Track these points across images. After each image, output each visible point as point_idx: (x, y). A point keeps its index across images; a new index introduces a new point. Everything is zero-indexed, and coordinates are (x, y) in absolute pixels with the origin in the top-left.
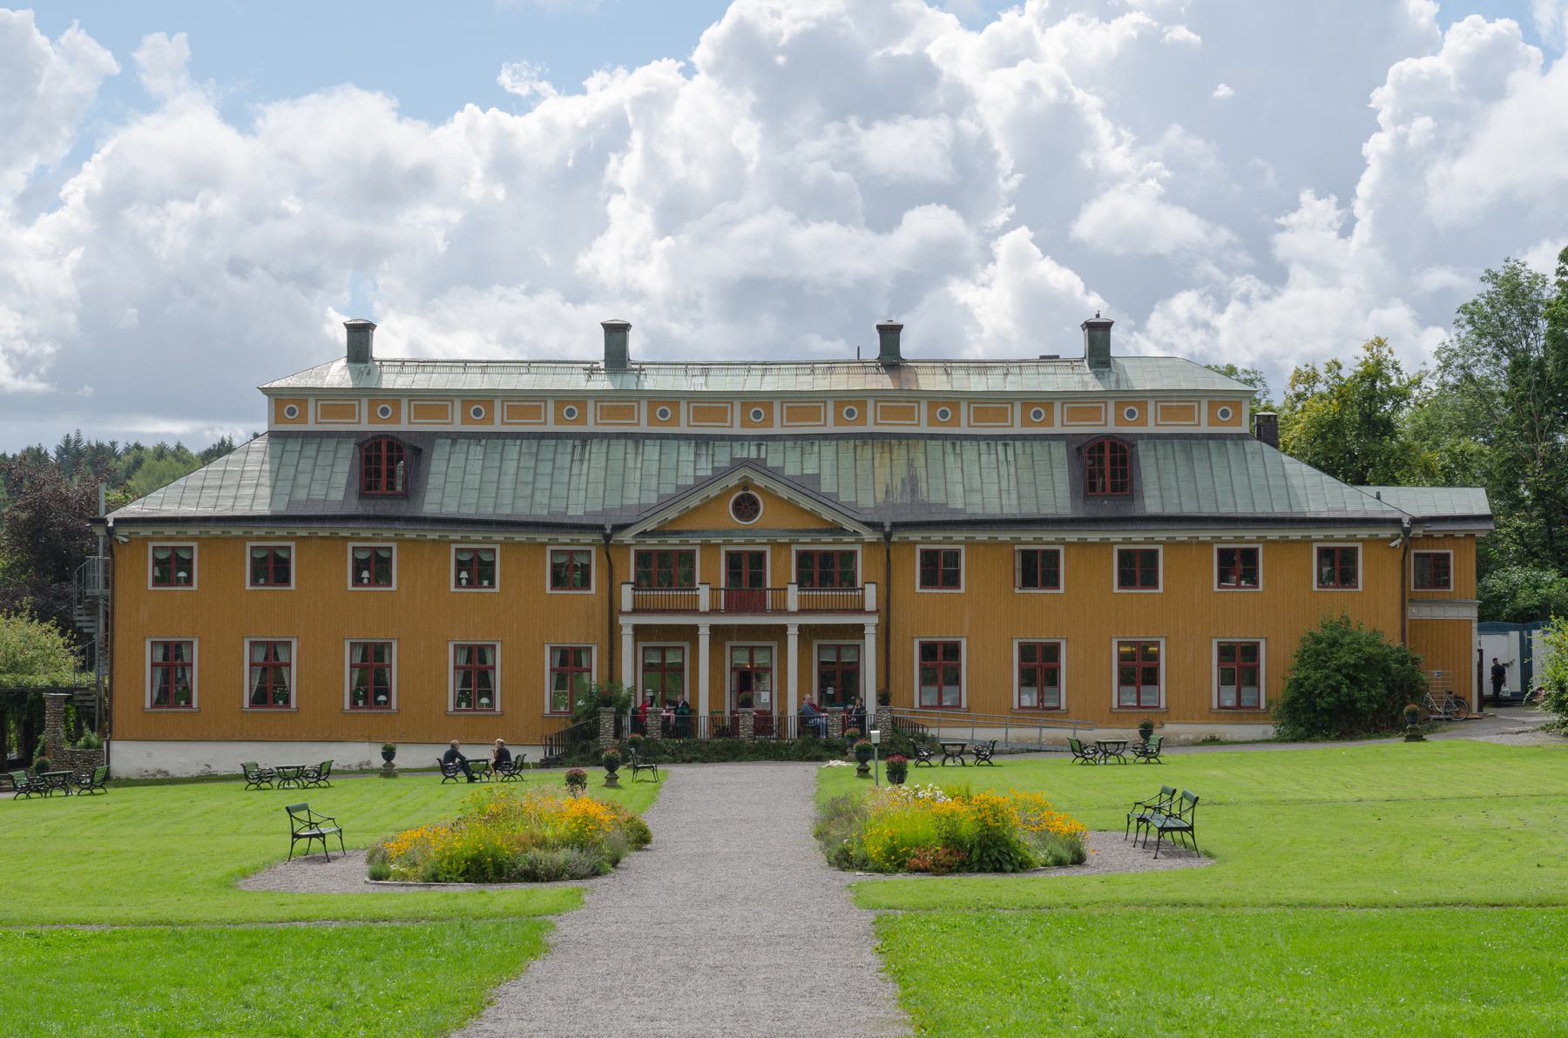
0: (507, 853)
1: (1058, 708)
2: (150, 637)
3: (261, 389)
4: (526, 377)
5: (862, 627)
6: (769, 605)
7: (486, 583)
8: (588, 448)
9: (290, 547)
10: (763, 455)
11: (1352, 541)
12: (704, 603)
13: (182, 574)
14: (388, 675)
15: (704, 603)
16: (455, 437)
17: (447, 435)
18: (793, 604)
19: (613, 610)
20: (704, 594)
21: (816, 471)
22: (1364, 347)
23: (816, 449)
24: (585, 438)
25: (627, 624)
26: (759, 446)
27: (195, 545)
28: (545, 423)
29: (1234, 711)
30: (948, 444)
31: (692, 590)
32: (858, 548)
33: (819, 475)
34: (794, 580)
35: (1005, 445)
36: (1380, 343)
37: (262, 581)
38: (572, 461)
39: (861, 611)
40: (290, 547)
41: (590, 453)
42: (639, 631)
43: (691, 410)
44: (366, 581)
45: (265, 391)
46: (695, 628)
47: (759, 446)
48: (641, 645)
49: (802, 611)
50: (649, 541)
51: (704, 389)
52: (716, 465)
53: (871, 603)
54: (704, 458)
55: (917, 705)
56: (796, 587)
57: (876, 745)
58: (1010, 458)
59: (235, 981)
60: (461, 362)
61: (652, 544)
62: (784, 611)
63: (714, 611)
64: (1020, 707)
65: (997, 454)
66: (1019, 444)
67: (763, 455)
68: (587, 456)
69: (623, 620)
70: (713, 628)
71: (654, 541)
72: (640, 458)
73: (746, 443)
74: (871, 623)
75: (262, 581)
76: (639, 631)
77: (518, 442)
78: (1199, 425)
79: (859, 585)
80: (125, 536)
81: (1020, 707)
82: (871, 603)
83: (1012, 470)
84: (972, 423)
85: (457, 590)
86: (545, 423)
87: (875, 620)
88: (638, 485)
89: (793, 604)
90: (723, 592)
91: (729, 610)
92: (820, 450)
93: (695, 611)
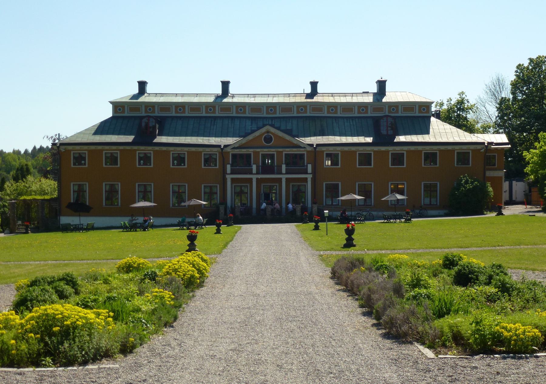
0: (130, 261)
1: (371, 205)
2: (203, 184)
3: (110, 102)
4: (196, 98)
5: (307, 179)
6: (276, 171)
7: (183, 164)
8: (216, 121)
9: (118, 153)
10: (273, 123)
11: (468, 150)
12: (254, 171)
13: (83, 162)
14: (85, 196)
15: (254, 171)
16: (173, 118)
17: (171, 117)
18: (284, 171)
19: (224, 173)
20: (254, 167)
21: (291, 128)
22: (458, 94)
23: (291, 121)
24: (215, 118)
25: (229, 177)
26: (272, 121)
27: (86, 152)
28: (142, 113)
29: (429, 206)
30: (345, 120)
31: (250, 167)
32: (470, 151)
33: (292, 129)
34: (284, 163)
35: (353, 120)
36: (463, 93)
37: (460, 164)
38: (211, 125)
39: (306, 173)
40: (118, 153)
41: (217, 122)
42: (233, 180)
43: (384, 110)
44: (142, 164)
45: (111, 102)
46: (251, 179)
47: (272, 121)
48: (234, 185)
49: (287, 173)
50: (236, 150)
51: (254, 102)
52: (258, 126)
53: (310, 169)
54: (254, 124)
55: (324, 204)
56: (285, 165)
57: (327, 217)
58: (354, 124)
59: (393, 312)
60: (267, 94)
61: (237, 151)
62: (281, 173)
63: (257, 173)
64: (358, 205)
65: (350, 122)
66: (357, 119)
67: (273, 123)
68: (216, 124)
69: (227, 176)
70: (287, 179)
71: (238, 150)
72: (233, 125)
73: (268, 119)
74: (309, 177)
75: (432, 164)
76: (233, 180)
77: (193, 119)
78: (354, 114)
79: (306, 164)
80: (63, 149)
81: (424, 205)
82: (310, 169)
83: (355, 127)
84: (311, 112)
85: (204, 167)
86: (232, 113)
87: (311, 176)
88: (232, 133)
89: (284, 171)
90: (260, 167)
91: (263, 173)
92: (292, 122)
93: (251, 173)
